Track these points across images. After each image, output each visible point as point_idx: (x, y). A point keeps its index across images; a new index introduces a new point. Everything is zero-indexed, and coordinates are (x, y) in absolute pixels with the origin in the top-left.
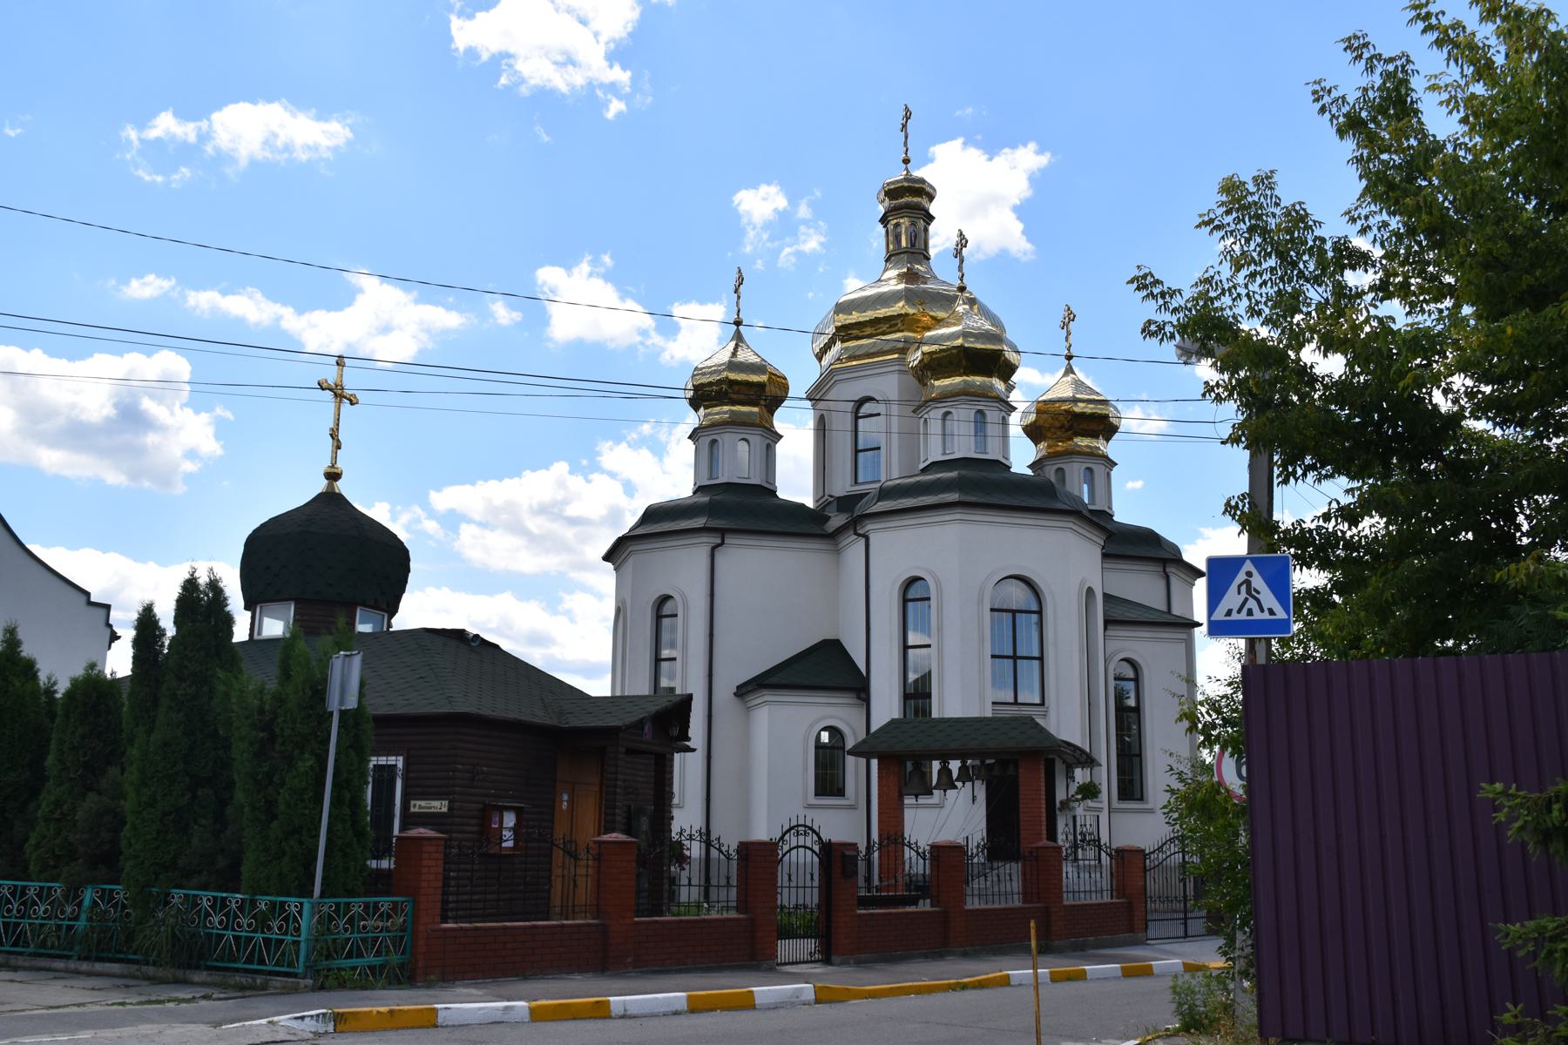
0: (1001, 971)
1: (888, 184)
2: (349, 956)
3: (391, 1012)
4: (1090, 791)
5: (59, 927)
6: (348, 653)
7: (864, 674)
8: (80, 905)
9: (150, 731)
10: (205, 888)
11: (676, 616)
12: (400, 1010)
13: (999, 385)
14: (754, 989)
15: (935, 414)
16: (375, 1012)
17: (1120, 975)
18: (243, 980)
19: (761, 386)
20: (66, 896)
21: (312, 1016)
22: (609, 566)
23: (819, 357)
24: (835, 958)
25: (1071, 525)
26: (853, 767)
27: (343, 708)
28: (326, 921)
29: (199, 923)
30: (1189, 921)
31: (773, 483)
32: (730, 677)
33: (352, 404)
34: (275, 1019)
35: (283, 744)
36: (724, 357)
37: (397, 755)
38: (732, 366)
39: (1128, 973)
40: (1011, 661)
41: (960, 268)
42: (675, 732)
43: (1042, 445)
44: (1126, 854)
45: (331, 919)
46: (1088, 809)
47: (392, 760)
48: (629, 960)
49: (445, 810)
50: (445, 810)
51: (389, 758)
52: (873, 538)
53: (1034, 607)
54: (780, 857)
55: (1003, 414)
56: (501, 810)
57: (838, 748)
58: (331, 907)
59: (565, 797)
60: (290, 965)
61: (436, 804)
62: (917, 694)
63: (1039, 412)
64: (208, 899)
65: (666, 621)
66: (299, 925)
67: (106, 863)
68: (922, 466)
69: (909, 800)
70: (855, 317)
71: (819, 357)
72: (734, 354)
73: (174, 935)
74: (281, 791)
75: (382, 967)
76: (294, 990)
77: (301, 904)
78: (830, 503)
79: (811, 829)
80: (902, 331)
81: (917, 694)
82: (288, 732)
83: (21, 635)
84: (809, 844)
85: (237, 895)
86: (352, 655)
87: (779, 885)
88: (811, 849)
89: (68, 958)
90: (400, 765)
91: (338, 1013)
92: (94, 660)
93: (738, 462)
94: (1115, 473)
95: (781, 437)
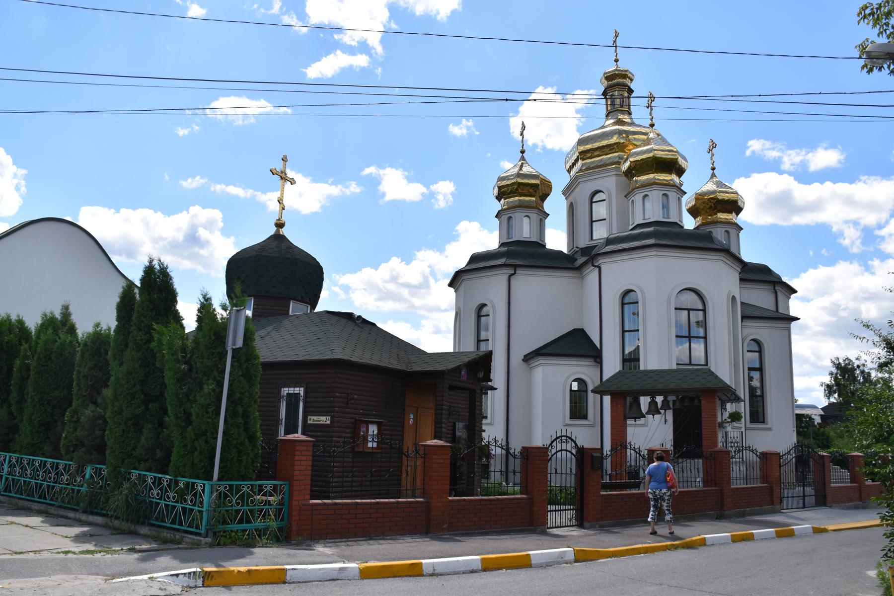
0: (699, 535)
1: (606, 73)
2: (241, 522)
3: (249, 571)
4: (735, 417)
5: (73, 490)
6: (239, 308)
7: (599, 348)
8: (84, 477)
9: (121, 364)
10: (149, 471)
11: (489, 315)
12: (256, 570)
13: (674, 177)
14: (531, 552)
15: (638, 198)
16: (236, 571)
17: (775, 536)
18: (169, 535)
19: (537, 185)
20: (77, 471)
21: (185, 574)
22: (452, 290)
23: (569, 171)
24: (586, 524)
25: (722, 258)
26: (592, 399)
27: (234, 347)
28: (222, 497)
29: (146, 494)
30: (802, 495)
31: (544, 241)
32: (519, 351)
33: (292, 184)
34: (155, 575)
35: (197, 373)
36: (516, 170)
37: (300, 387)
38: (519, 175)
39: (780, 535)
40: (692, 335)
41: (651, 114)
42: (481, 375)
43: (698, 219)
44: (768, 456)
45: (226, 496)
46: (734, 428)
47: (297, 390)
48: (445, 526)
49: (328, 422)
50: (328, 422)
51: (290, 389)
52: (603, 267)
53: (701, 307)
54: (549, 457)
55: (678, 196)
56: (367, 423)
57: (583, 391)
58: (226, 487)
59: (412, 416)
60: (197, 528)
61: (323, 418)
62: (631, 360)
63: (697, 199)
64: (151, 478)
65: (483, 319)
66: (203, 499)
67: (98, 451)
68: (631, 227)
69: (630, 422)
70: (589, 147)
71: (569, 171)
72: (521, 169)
73: (127, 501)
74: (194, 405)
75: (266, 529)
76: (197, 545)
77: (204, 485)
78: (577, 251)
79: (570, 438)
80: (617, 152)
81: (631, 360)
82: (199, 365)
83: (72, 309)
84: (569, 449)
85: (167, 477)
86: (240, 310)
87: (549, 472)
88: (570, 452)
89: (76, 510)
90: (302, 393)
91: (207, 572)
92: (98, 321)
93: (525, 230)
94: (742, 234)
95: (548, 215)
